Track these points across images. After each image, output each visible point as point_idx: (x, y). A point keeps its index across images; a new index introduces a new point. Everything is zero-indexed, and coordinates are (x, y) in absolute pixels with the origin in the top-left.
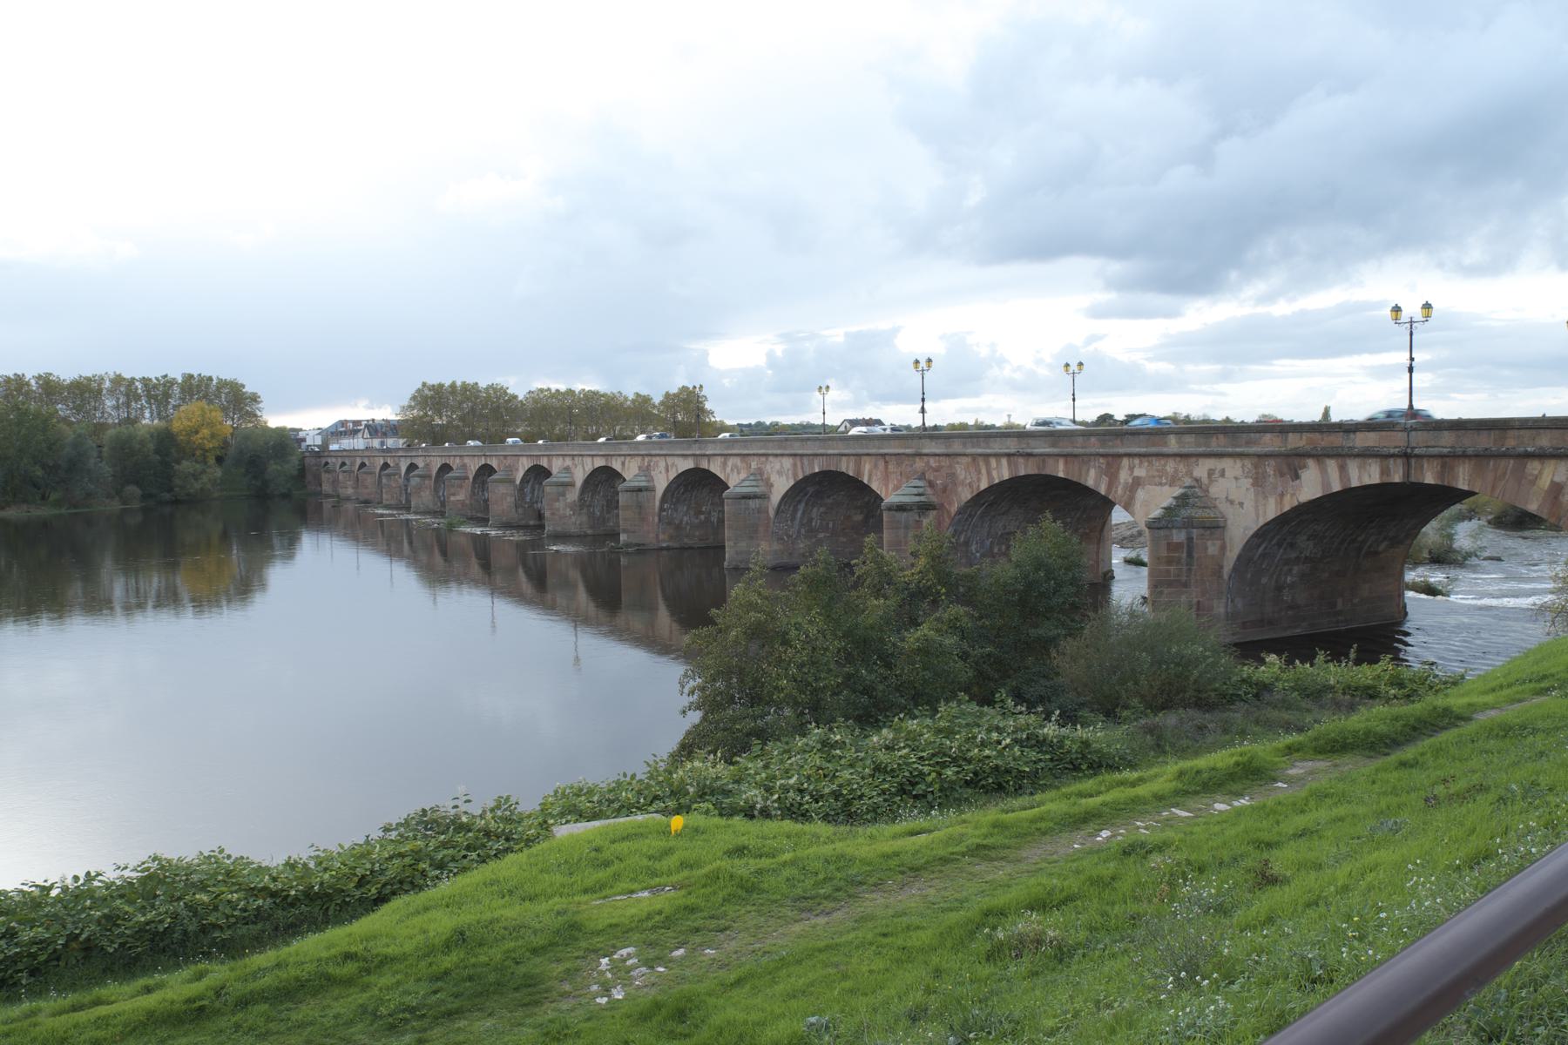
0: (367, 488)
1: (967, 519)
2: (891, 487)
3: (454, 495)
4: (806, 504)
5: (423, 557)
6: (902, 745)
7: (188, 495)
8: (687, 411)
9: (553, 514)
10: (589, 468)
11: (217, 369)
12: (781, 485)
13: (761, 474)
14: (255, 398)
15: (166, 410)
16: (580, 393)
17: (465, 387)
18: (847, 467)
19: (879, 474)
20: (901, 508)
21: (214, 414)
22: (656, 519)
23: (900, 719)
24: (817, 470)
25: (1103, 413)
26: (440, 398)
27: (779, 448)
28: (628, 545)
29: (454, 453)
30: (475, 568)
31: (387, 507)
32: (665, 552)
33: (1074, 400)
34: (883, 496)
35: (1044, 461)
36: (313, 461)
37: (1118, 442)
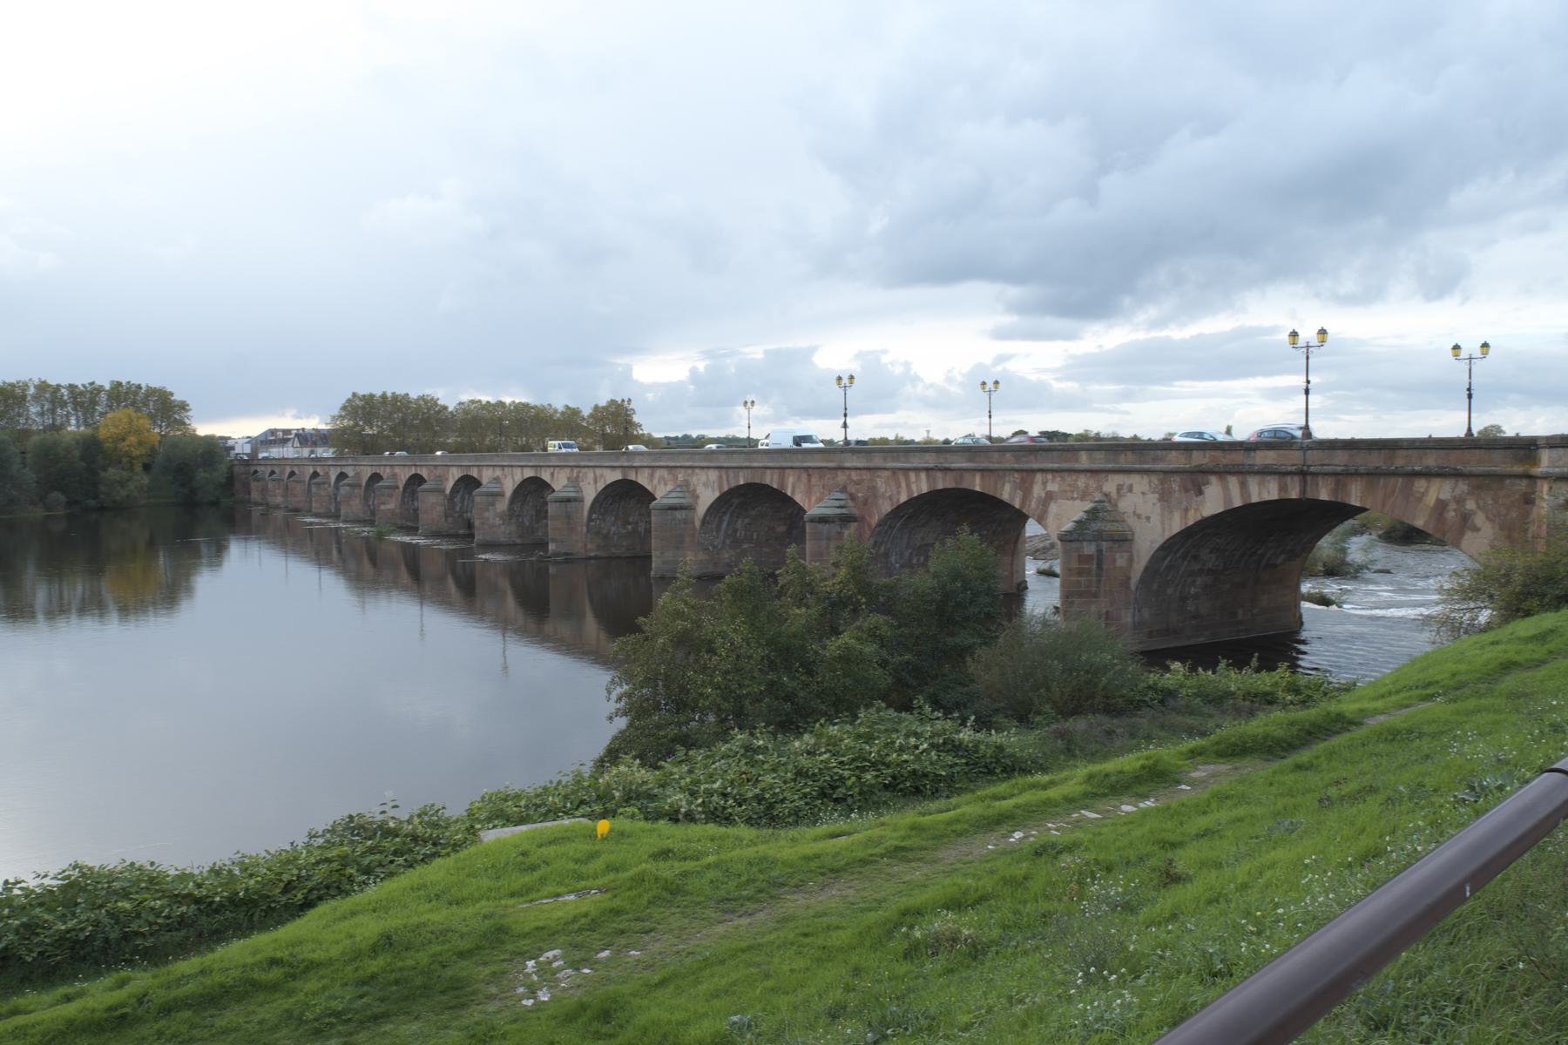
1: (886, 532)
2: (813, 499)
3: (384, 503)
4: (731, 515)
6: (823, 750)
8: (615, 425)
9: (483, 523)
10: (518, 478)
11: (146, 376)
12: (707, 497)
14: (183, 406)
16: (510, 405)
17: (395, 397)
18: (772, 480)
19: (802, 487)
20: (823, 520)
22: (585, 529)
23: (821, 725)
24: (742, 483)
28: (556, 555)
30: (405, 577)
31: (317, 515)
32: (592, 561)
36: (242, 469)
37: (1032, 457)
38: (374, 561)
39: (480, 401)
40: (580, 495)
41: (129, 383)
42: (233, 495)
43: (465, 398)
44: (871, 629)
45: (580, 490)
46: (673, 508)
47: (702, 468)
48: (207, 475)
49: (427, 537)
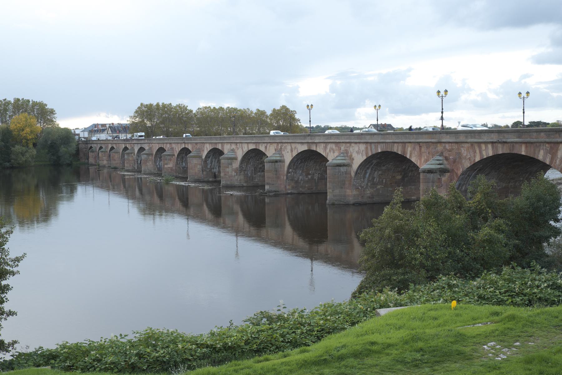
0: (115, 160)
1: (466, 178)
2: (423, 160)
3: (167, 164)
4: (372, 169)
5: (148, 198)
6: (489, 286)
7: (18, 164)
8: (285, 120)
9: (225, 175)
10: (246, 149)
11: (33, 96)
12: (358, 159)
13: (347, 153)
14: (52, 112)
15: (5, 118)
16: (226, 109)
17: (164, 106)
18: (397, 150)
19: (416, 153)
20: (430, 171)
21: (32, 120)
22: (285, 177)
23: (485, 274)
24: (380, 151)
25: (516, 121)
26: (151, 111)
27: (358, 139)
28: (269, 192)
29: (166, 142)
30: (178, 204)
31: (128, 171)
32: (289, 196)
33: (524, 113)
34: (418, 165)
35: (513, 146)
36: (84, 146)
37: (557, 135)
38: (161, 196)
39: (210, 107)
40: (282, 158)
41: (23, 99)
42: (79, 160)
43: (202, 105)
44: (496, 226)
45: (282, 156)
46: (339, 165)
47: (356, 143)
48: (66, 149)
49: (192, 182)
